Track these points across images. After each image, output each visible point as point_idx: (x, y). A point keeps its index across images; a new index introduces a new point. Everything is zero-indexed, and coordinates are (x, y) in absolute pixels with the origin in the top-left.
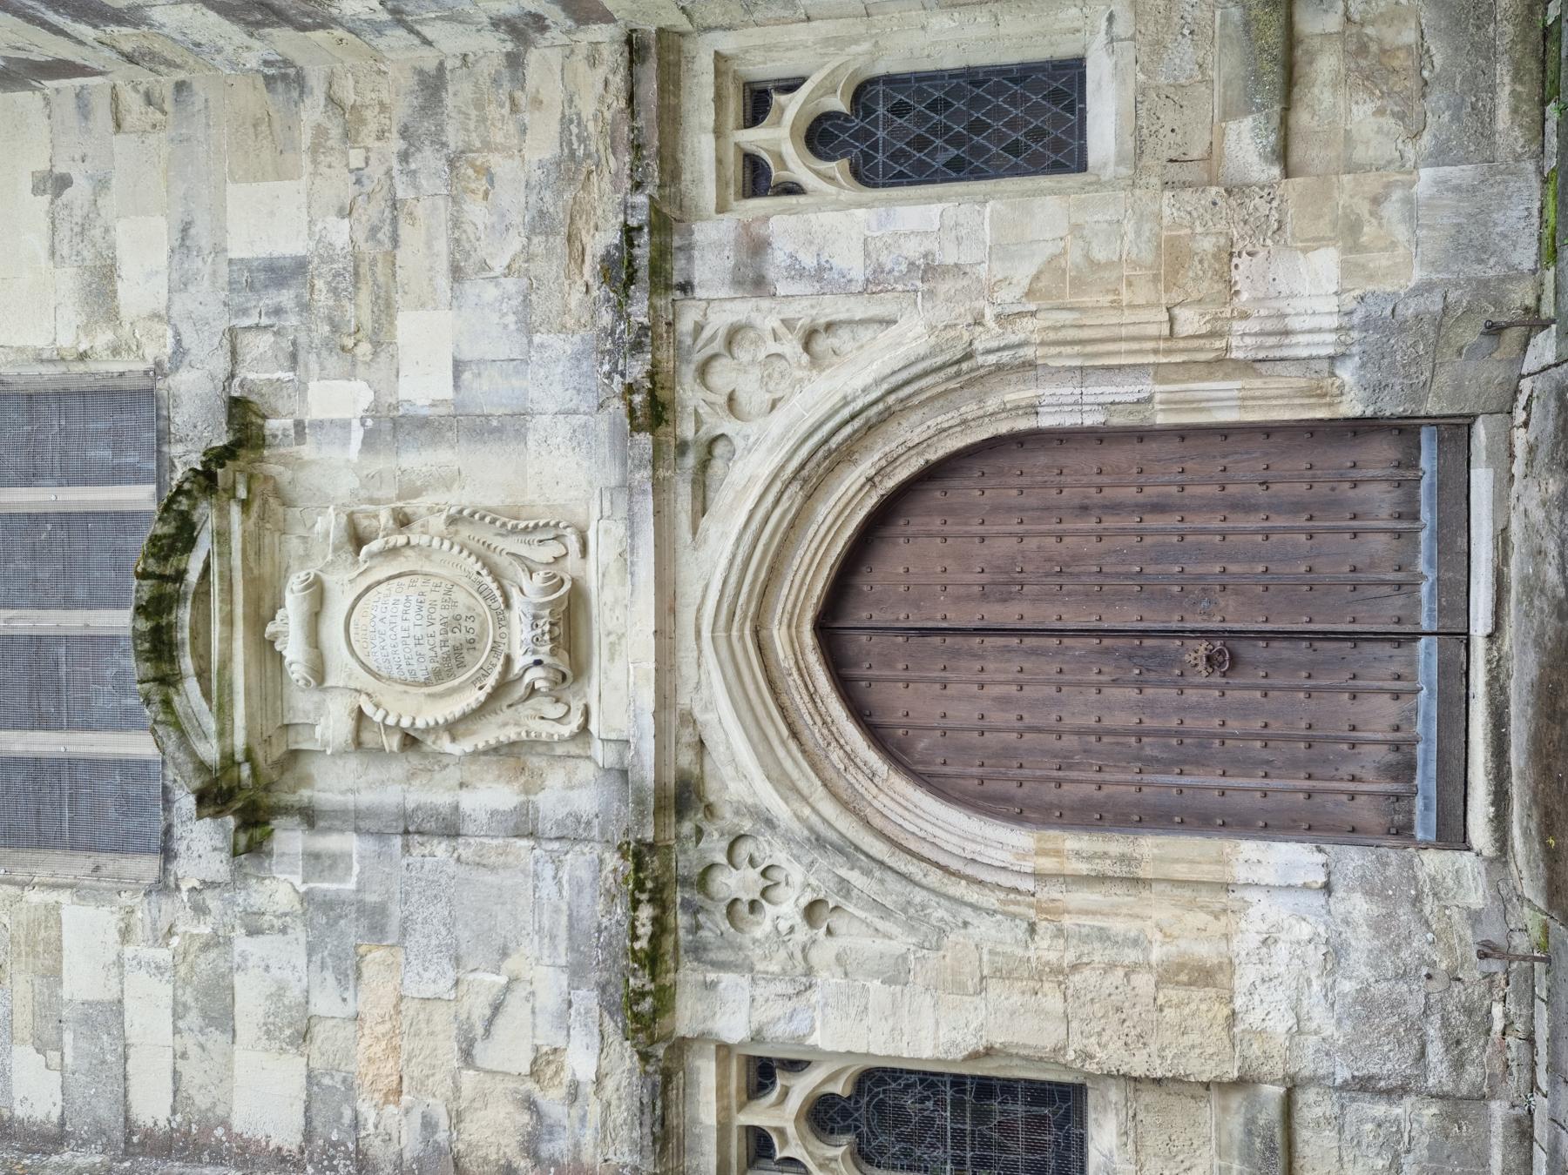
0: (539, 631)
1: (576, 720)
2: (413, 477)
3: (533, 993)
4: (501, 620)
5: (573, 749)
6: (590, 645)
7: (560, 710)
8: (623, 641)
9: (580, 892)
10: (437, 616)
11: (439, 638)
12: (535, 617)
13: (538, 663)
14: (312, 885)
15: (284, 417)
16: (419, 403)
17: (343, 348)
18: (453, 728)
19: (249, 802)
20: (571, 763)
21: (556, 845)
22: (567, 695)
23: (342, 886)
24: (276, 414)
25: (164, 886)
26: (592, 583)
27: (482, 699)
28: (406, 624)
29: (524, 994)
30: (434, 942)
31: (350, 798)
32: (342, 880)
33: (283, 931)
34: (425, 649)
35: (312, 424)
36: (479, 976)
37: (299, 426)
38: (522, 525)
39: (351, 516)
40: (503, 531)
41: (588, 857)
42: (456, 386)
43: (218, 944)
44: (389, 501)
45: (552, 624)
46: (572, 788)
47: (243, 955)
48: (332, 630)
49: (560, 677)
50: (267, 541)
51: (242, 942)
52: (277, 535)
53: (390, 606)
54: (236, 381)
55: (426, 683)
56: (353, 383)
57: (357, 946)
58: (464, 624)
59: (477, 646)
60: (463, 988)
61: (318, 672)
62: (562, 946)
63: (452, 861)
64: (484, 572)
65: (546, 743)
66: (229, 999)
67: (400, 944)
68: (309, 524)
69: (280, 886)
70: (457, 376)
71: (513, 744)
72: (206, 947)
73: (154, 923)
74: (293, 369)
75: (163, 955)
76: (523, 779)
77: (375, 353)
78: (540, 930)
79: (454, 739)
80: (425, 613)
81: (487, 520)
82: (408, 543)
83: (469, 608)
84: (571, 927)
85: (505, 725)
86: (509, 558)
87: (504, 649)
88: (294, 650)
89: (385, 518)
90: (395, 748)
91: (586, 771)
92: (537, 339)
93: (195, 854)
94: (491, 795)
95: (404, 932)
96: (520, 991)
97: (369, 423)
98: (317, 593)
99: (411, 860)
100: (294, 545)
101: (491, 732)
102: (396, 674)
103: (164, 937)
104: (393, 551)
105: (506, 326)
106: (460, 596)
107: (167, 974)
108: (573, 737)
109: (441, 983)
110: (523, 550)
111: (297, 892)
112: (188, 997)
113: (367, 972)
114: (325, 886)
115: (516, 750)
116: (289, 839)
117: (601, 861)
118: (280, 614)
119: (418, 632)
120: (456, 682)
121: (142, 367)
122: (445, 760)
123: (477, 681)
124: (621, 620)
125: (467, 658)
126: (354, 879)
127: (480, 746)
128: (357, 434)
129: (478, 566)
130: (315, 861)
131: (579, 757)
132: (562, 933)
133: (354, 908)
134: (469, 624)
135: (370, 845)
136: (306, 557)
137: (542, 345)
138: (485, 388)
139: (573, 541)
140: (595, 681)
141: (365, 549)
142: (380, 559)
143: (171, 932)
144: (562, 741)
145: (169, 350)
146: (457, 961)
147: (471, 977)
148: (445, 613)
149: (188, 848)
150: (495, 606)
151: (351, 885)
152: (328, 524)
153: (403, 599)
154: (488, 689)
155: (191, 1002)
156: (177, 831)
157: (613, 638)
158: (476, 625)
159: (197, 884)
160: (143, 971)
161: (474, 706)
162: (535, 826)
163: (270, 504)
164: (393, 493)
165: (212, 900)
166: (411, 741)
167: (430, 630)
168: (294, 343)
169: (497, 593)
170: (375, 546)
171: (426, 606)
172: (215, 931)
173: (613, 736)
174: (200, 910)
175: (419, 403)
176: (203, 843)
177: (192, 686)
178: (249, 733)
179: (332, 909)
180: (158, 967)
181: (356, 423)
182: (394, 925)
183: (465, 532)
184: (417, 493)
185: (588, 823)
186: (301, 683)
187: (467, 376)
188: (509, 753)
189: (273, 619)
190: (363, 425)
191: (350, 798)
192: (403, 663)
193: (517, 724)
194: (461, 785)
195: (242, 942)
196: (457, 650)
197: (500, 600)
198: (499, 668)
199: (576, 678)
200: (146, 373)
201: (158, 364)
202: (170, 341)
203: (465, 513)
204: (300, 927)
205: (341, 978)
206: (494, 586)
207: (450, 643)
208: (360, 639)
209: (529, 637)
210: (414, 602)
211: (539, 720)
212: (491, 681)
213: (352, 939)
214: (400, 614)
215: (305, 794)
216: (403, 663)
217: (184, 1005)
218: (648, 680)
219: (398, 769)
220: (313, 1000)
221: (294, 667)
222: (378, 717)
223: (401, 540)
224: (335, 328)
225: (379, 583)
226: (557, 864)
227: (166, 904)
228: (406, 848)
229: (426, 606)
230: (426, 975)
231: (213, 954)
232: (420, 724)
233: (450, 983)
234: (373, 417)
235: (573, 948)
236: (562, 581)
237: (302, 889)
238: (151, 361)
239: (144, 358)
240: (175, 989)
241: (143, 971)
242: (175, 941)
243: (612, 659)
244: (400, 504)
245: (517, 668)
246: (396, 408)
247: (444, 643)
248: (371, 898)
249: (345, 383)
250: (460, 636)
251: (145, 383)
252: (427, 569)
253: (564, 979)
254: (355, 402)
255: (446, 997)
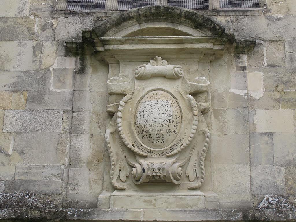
0: (157, 171)
1: (118, 185)
2: (223, 116)
3: (4, 165)
4: (162, 154)
5: (106, 184)
6: (150, 191)
7: (123, 178)
8: (152, 206)
9: (46, 185)
10: (164, 128)
11: (155, 128)
12: (163, 169)
13: (144, 170)
14: (52, 72)
15: (248, 62)
16: (255, 118)
17: (277, 86)
18: (116, 133)
19: (87, 49)
20: (101, 182)
21: (65, 175)
22: (130, 181)
23: (52, 85)
24: (249, 58)
25: (54, 12)
26: (178, 193)
27: (129, 146)
28: (161, 115)
29: (4, 161)
30: (27, 123)
31: (88, 89)
32: (54, 86)
33: (34, 61)
34: (150, 123)
35: (245, 73)
36: (12, 142)
37: (244, 68)
38: (203, 163)
39: (206, 91)
40: (200, 155)
41: (60, 189)
42: (262, 134)
43: (30, 34)
44: (213, 105)
45: (160, 176)
46: (90, 182)
47: (25, 44)
48: (158, 84)
49: (138, 179)
50: (195, 56)
51: (30, 44)
52: (198, 60)
53: (168, 108)
54: (262, 42)
55: (135, 122)
56: (262, 90)
57: (27, 91)
58: (160, 139)
59: (151, 144)
60: (8, 135)
61: (141, 78)
62: (23, 178)
63: (60, 131)
64: (182, 147)
65: (109, 172)
66: (7, 39)
67: (27, 109)
68: (203, 73)
69: (54, 60)
70: (266, 134)
71: (109, 158)
72: (29, 30)
73: (39, 9)
74: (268, 65)
75: (26, 13)
76: (94, 161)
77: (275, 100)
78: (30, 168)
79: (112, 133)
80: (165, 123)
81: (205, 148)
82: (195, 116)
83: (167, 141)
84: (30, 181)
85: (117, 154)
86: (188, 157)
87: (149, 155)
88: (150, 67)
89: (205, 105)
90: (108, 109)
91: (97, 188)
92: (283, 169)
93: (67, 25)
94: (85, 147)
95: (31, 111)
96: (5, 160)
97: (246, 97)
98: (173, 78)
99: (62, 113)
100: (194, 67)
101: (114, 148)
102: (140, 110)
103: (34, 13)
104: (191, 109)
105: (288, 155)
106: (171, 137)
107: (19, 15)
108: (112, 184)
109: (10, 126)
110: (192, 163)
111: (50, 67)
112: (10, 23)
113: (15, 95)
114: (52, 78)
115: (106, 159)
116: (71, 63)
117: (58, 195)
118: (165, 62)
119: (157, 120)
120: (136, 135)
121: (268, 4)
122: (103, 128)
123: (135, 144)
124: (161, 206)
125: (146, 140)
126: (54, 90)
127: (109, 145)
128: (241, 92)
129: (185, 145)
130: (60, 72)
131: (103, 186)
132: (29, 178)
133: (42, 90)
134: (160, 141)
135: (68, 97)
136: (189, 72)
137: (280, 171)
138: (261, 146)
139: (196, 184)
140: (135, 193)
141: (192, 97)
142: (188, 104)
143: (36, 16)
144: (111, 179)
145: (275, 15)
146: (18, 133)
147: (12, 138)
148: (165, 131)
149: (69, 23)
150: (168, 151)
151: (52, 89)
152: (202, 81)
153: (171, 113)
154: (133, 148)
155: (7, 24)
156: (77, 18)
157: (154, 202)
158: (160, 144)
159: (55, 26)
160: (20, 5)
161: (126, 143)
162: (74, 166)
163: (210, 59)
164: (216, 107)
165: (49, 32)
166: (111, 115)
167: (158, 125)
168: (279, 66)
169: (173, 153)
170: (194, 102)
171: (168, 123)
172: (36, 33)
173: (112, 202)
174: (44, 28)
175: (255, 118)
176: (72, 28)
177: (136, 28)
178: (115, 50)
179: (42, 81)
180: (22, 11)
181: (246, 91)
182: (35, 106)
183: (200, 138)
184: (216, 117)
185: (74, 189)
186: (137, 71)
187: (266, 138)
188: (104, 156)
189: (163, 59)
190: (245, 95)
191: (88, 89)
192: (144, 113)
193: (117, 160)
194: (92, 135)
195: (30, 44)
196: (149, 136)
197: (170, 154)
198: (142, 153)
199: (136, 185)
200: (265, 5)
201: (269, 11)
202: (279, 16)
203: (207, 139)
204: (35, 68)
205: (14, 85)
206: (176, 151)
207: (152, 133)
208: (156, 95)
209: (154, 167)
210: (170, 118)
211: (119, 172)
212: (136, 150)
213: (30, 89)
214: (165, 112)
215: (89, 70)
216: (144, 113)
217: (6, 21)
218: (136, 217)
219: (99, 108)
220: (5, 73)
221: (143, 68)
222: (122, 103)
223: (196, 113)
224: (286, 83)
225: (178, 103)
226: (57, 176)
227: (47, 14)
228: (65, 112)
229: (168, 123)
230: (13, 120)
231: (26, 32)
232: (119, 120)
233: (10, 130)
234: (248, 99)
235: (22, 182)
236: (178, 180)
237: (51, 69)
238: (270, 8)
239: (271, 5)
240: (13, 18)
241: (20, 5)
242: (32, 18)
243: (145, 201)
244: (211, 110)
245: (142, 161)
246: (252, 108)
247: (152, 130)
248: (46, 97)
249: (262, 87)
250: (154, 136)
251: (261, 5)
252: (183, 123)
253: (9, 178)
254: (254, 91)
255: (4, 128)
